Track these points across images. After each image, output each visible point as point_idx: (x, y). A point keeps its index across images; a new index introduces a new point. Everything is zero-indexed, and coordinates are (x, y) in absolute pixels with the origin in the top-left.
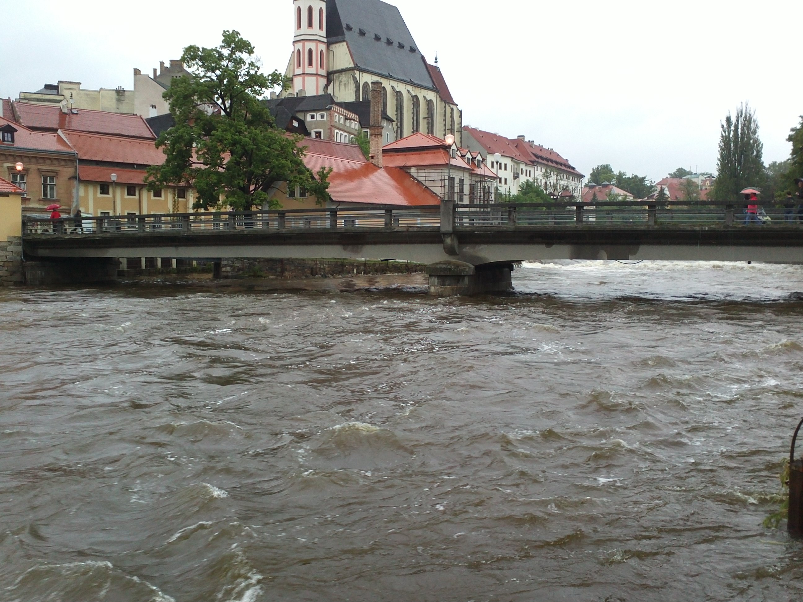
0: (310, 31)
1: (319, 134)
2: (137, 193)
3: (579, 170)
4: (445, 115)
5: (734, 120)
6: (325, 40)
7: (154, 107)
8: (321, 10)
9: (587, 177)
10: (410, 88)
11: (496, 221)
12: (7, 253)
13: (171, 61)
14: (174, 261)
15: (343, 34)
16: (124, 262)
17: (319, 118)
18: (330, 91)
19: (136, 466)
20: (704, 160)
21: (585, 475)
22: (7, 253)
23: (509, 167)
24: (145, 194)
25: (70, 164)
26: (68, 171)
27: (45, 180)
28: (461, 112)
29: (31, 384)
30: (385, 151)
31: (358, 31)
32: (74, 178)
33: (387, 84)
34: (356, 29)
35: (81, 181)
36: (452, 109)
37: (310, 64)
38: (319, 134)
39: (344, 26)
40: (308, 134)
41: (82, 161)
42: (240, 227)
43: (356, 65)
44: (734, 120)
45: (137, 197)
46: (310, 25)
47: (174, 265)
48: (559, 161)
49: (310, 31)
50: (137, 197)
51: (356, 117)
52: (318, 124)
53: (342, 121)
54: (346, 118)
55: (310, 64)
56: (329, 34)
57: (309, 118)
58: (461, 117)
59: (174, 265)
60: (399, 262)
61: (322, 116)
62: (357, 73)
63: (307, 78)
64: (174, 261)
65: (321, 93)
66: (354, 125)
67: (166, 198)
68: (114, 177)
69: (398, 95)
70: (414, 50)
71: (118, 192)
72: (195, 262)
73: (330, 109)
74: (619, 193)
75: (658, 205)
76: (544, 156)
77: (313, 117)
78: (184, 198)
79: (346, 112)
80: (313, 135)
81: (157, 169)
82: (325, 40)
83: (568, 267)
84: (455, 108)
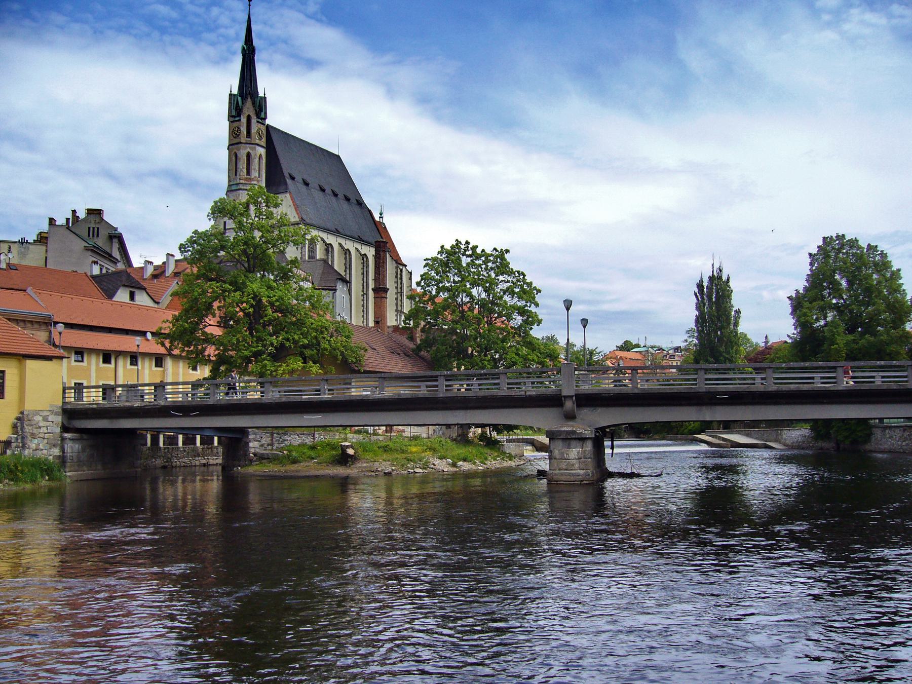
2: (113, 361)
5: (705, 284)
10: (359, 246)
13: (88, 210)
15: (286, 184)
19: (13, 645)
20: (672, 324)
21: (870, 630)
24: (121, 362)
25: (43, 327)
28: (411, 273)
31: (301, 181)
34: (299, 178)
36: (401, 270)
39: (287, 175)
42: (221, 397)
44: (705, 284)
45: (112, 366)
50: (112, 366)
60: (748, 435)
67: (89, 364)
69: (347, 252)
70: (360, 203)
71: (94, 359)
78: (161, 366)
84: (404, 269)
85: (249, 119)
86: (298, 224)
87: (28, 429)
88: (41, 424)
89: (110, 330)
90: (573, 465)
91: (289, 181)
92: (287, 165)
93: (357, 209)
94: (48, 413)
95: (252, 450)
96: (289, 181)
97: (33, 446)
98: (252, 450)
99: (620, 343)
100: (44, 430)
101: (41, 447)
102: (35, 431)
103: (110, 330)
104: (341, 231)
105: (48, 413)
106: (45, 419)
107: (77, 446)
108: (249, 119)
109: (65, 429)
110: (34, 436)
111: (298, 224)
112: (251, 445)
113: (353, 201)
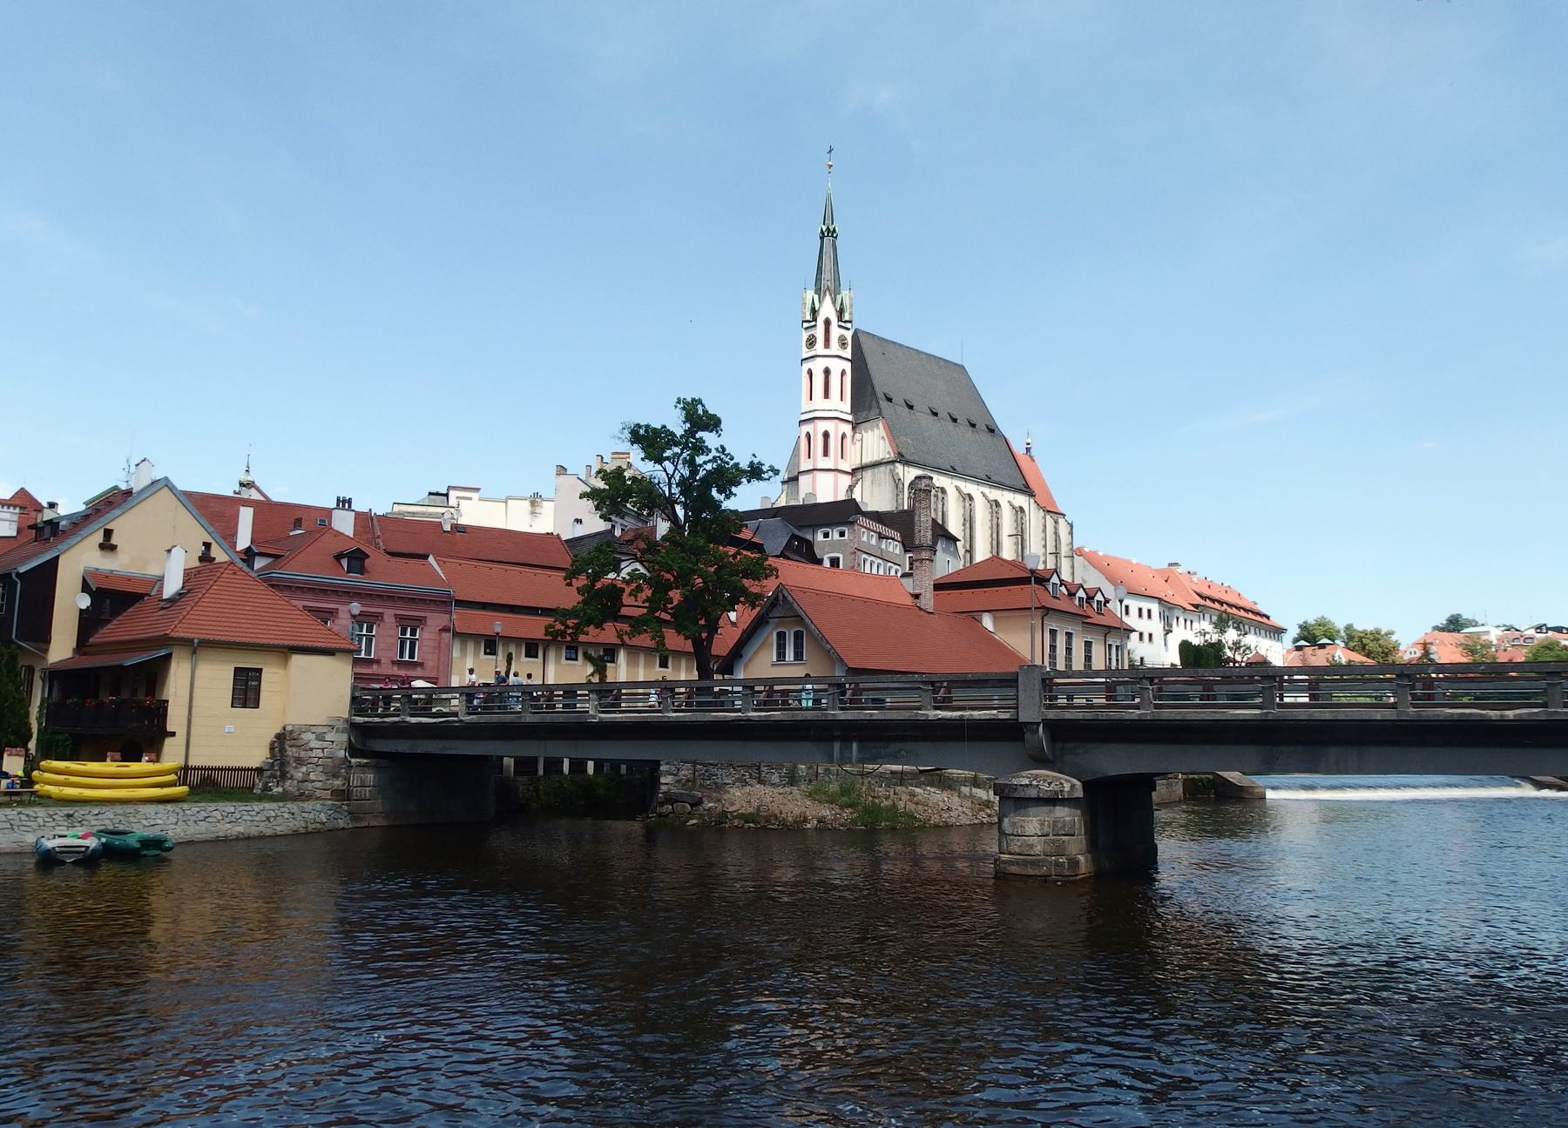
0: (826, 404)
1: (835, 562)
3: (1276, 620)
4: (1044, 531)
6: (850, 418)
7: (579, 521)
8: (843, 373)
9: (1294, 632)
10: (986, 490)
11: (1139, 710)
12: (325, 744)
14: (591, 764)
16: (509, 762)
17: (836, 536)
18: (857, 496)
22: (325, 744)
23: (1155, 614)
26: (436, 620)
27: (404, 632)
29: (846, 888)
30: (938, 587)
32: (445, 629)
33: (939, 480)
35: (456, 634)
37: (826, 453)
38: (835, 562)
40: (819, 562)
41: (461, 603)
43: (900, 454)
46: (826, 395)
47: (566, 769)
48: (1241, 604)
49: (826, 404)
51: (898, 536)
52: (834, 546)
53: (873, 542)
54: (881, 537)
55: (826, 453)
56: (856, 406)
57: (820, 537)
58: (1071, 533)
59: (566, 769)
61: (842, 534)
62: (899, 467)
63: (819, 475)
64: (591, 764)
65: (842, 497)
66: (894, 548)
68: (498, 628)
72: (624, 768)
73: (852, 523)
74: (1341, 655)
75: (1417, 676)
76: (1216, 596)
77: (826, 535)
79: (880, 528)
80: (827, 563)
81: (573, 613)
82: (850, 418)
83: (297, 824)
85: (827, 322)
86: (893, 462)
87: (291, 752)
88: (312, 745)
89: (484, 606)
90: (1032, 846)
91: (884, 404)
92: (882, 378)
93: (987, 437)
94: (325, 730)
95: (664, 788)
96: (884, 404)
97: (299, 775)
98: (664, 788)
99: (1442, 620)
100: (319, 753)
101: (312, 776)
102: (303, 754)
103: (484, 606)
104: (908, 457)
105: (325, 730)
106: (320, 737)
107: (370, 777)
108: (827, 322)
109: (353, 750)
110: (300, 761)
111: (893, 462)
112: (663, 780)
113: (981, 425)
